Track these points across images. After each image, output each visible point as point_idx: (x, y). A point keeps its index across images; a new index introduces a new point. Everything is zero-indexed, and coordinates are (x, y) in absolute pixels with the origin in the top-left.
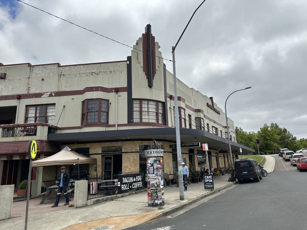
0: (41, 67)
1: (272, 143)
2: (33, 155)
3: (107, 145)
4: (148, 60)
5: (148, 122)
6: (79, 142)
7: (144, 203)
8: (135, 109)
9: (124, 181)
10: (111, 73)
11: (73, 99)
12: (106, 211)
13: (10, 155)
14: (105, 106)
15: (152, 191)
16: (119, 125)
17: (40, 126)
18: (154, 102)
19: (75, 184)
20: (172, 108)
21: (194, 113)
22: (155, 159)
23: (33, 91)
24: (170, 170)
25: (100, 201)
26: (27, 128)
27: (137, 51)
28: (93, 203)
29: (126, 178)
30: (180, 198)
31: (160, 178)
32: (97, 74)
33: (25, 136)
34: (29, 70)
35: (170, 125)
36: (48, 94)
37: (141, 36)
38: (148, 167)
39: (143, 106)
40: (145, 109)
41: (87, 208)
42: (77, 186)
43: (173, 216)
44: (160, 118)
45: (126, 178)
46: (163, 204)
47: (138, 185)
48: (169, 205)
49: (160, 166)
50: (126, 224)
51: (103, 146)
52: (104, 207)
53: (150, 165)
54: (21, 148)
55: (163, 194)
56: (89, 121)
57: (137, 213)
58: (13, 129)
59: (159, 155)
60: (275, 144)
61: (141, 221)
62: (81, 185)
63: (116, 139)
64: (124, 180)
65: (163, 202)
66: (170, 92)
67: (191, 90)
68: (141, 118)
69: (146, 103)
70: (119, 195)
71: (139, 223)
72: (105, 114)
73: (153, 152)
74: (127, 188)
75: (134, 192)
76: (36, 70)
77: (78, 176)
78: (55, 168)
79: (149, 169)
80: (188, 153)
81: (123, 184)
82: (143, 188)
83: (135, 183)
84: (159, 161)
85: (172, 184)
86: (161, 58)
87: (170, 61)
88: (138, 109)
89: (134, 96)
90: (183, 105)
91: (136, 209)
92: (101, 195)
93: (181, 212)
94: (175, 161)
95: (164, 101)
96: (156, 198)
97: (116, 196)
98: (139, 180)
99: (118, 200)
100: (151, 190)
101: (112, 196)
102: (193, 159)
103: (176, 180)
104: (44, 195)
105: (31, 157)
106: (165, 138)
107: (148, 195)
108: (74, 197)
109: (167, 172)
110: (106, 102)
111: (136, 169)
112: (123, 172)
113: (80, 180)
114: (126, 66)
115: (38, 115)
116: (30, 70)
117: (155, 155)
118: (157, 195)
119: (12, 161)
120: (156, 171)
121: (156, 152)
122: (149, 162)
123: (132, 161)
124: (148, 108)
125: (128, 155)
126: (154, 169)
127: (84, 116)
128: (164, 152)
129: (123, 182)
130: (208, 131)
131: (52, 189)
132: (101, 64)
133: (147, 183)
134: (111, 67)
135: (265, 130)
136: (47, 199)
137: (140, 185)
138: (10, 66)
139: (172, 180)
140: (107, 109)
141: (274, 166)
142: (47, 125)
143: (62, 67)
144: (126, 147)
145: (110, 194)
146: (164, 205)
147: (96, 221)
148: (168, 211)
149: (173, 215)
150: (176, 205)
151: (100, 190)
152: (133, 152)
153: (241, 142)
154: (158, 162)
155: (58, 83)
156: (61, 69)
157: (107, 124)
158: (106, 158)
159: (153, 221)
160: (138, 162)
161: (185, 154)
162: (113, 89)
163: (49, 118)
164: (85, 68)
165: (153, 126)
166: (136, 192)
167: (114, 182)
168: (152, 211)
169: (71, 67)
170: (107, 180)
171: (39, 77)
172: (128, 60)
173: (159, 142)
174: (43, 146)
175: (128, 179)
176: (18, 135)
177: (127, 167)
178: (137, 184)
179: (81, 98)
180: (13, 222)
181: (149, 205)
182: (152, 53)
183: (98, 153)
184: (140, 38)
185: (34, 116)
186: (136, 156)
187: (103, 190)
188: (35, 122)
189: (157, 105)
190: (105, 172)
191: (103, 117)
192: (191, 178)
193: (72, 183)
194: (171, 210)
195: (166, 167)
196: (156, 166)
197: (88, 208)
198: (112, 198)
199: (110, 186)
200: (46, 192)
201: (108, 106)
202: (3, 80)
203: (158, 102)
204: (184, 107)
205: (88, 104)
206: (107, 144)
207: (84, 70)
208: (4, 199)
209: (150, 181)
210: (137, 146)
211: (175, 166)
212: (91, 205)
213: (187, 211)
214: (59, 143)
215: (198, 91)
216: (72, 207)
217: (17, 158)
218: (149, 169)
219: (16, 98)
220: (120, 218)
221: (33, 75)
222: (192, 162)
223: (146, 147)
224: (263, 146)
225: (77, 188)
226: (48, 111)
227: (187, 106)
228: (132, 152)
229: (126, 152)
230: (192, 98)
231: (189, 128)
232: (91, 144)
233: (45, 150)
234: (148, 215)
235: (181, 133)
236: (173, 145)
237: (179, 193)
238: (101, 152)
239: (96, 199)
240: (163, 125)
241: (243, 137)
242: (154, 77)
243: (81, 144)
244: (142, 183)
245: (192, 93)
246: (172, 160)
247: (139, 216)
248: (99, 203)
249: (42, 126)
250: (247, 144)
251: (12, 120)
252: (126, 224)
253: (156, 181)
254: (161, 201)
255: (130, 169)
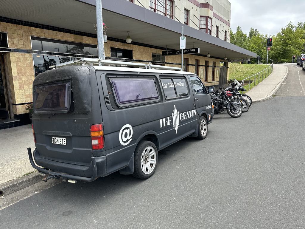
1: (293, 48)
60: (297, 51)
130: (187, 24)
135: (287, 32)
141: (281, 82)
153: (253, 48)
224: (280, 53)
227: (215, 15)
241: (257, 41)
250: (259, 50)
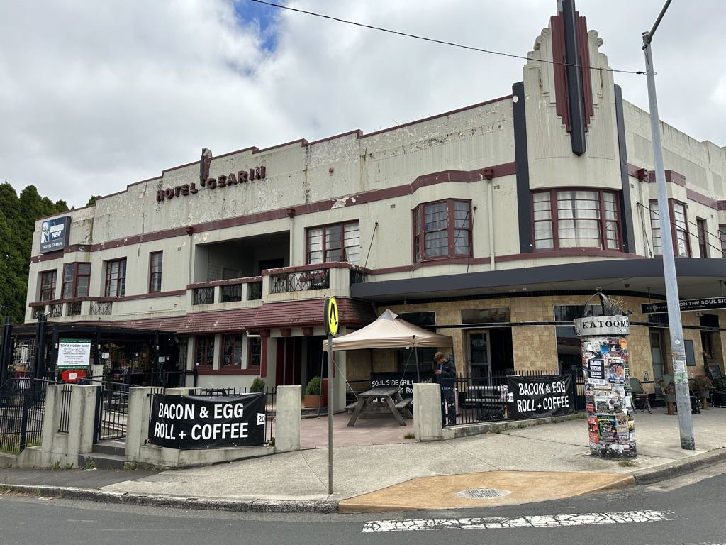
0: (326, 143)
2: (333, 328)
3: (472, 307)
4: (569, 82)
5: (575, 246)
6: (412, 301)
7: (578, 447)
8: (537, 216)
9: (522, 392)
10: (473, 134)
11: (393, 206)
12: (485, 456)
13: (287, 328)
14: (464, 215)
15: (601, 420)
16: (498, 259)
17: (334, 269)
18: (592, 193)
19: (415, 391)
20: (646, 203)
21: (714, 212)
22: (606, 340)
23: (315, 198)
24: (644, 369)
25: (469, 432)
26: (312, 273)
27: (538, 64)
28: (456, 434)
29: (526, 384)
30: (682, 443)
31: (621, 389)
32: (441, 141)
33: (309, 289)
34: (304, 154)
35: (640, 251)
36: (344, 200)
37: (546, 24)
38: (587, 360)
39: (561, 205)
40: (566, 214)
41: (444, 446)
42: (419, 394)
43: (664, 487)
44: (610, 235)
45: (526, 384)
46: (631, 454)
47: (559, 402)
48: (650, 459)
49: (620, 358)
50: (538, 490)
51: (463, 308)
52: (481, 446)
53: (591, 357)
54: (304, 314)
55: (631, 430)
56: (430, 253)
57: (562, 468)
58: (285, 276)
59: (616, 331)
61: (577, 489)
62: (426, 395)
63: (494, 292)
64: (521, 389)
65: (633, 449)
66: (635, 161)
67: (704, 148)
68: (556, 239)
69: (569, 197)
70: (514, 423)
71: (573, 493)
72: (463, 234)
73: (598, 325)
74: (530, 408)
75: (548, 420)
76: (317, 153)
77: (416, 373)
78: (366, 356)
79: (589, 365)
80: (699, 325)
81: (522, 397)
82: (571, 410)
83: (550, 398)
84: (618, 347)
85: (652, 407)
86: (606, 71)
87: (639, 73)
88: (546, 216)
89: (534, 184)
90: (679, 193)
91: (561, 459)
92: (468, 418)
93: (689, 480)
94: (658, 347)
95: (621, 188)
96: (611, 437)
97: (506, 425)
98: (560, 391)
99: (513, 433)
100: (598, 417)
101: (497, 423)
102: (714, 343)
103: (663, 396)
104: (353, 409)
105: (329, 331)
106: (627, 286)
107: (590, 428)
108: (412, 418)
109: (635, 374)
110: (464, 207)
111: (550, 364)
112: (515, 370)
113: (421, 382)
114: (512, 108)
115: (328, 247)
116: (307, 153)
117: (606, 331)
118: (614, 431)
119: (290, 340)
120: (610, 372)
121: (609, 324)
122: (589, 348)
123: (536, 344)
124: (574, 210)
125: (526, 330)
126: (603, 366)
127: (418, 243)
128: (631, 324)
129: (520, 394)
131: (367, 397)
132: (450, 116)
133: (587, 401)
134: (473, 120)
136: (360, 419)
137: (564, 404)
138: (270, 151)
139: (652, 396)
140: (468, 222)
142: (347, 266)
143: (366, 138)
144: (520, 311)
145: (489, 420)
146: (635, 456)
147: (468, 476)
148: (650, 472)
149: (664, 483)
150: (672, 461)
151: (464, 407)
152: (540, 324)
154: (613, 349)
155: (362, 175)
156: (364, 141)
157: (469, 258)
158: (473, 337)
159: (610, 494)
160: (554, 348)
161: (690, 330)
162: (480, 171)
163: (349, 252)
164: (414, 133)
165: (610, 257)
166: (555, 418)
167: (497, 393)
168: (603, 468)
169: (384, 134)
170: (478, 385)
171: (323, 166)
172: (514, 94)
173: (617, 297)
174: (343, 310)
175: (532, 388)
176: (297, 289)
177: (527, 358)
178: (556, 400)
179: (406, 204)
180: (306, 458)
181: (594, 454)
182: (580, 62)
183: (453, 324)
184: (544, 31)
185: (321, 249)
186: (546, 333)
187: (471, 407)
188: (325, 260)
189: (600, 201)
190: (473, 367)
191: (461, 242)
192: (710, 393)
193: (405, 387)
194: (657, 473)
195: (634, 361)
196: (607, 358)
197: (445, 446)
198: (497, 427)
199: (490, 400)
200: (356, 404)
201: (471, 216)
202: (261, 181)
203: (601, 192)
204: (683, 198)
205: (426, 213)
206: (473, 305)
207: (411, 137)
208: (287, 411)
209: (595, 396)
210: (549, 309)
211: (657, 361)
212: (451, 439)
213: (708, 480)
214: (373, 304)
215: (706, 143)
216: (411, 440)
217: (298, 333)
218: (589, 365)
219: (287, 215)
220: (522, 475)
221: (314, 164)
222: (710, 352)
223: (576, 313)
225: (418, 400)
226: (347, 236)
227: (692, 196)
228: (535, 324)
229: (521, 324)
230: (707, 170)
231: (63, 225)
232: (437, 304)
233: (347, 318)
234: (594, 476)
235: (679, 273)
236: (650, 305)
237: (677, 430)
238: (459, 322)
239: (461, 427)
240: (620, 252)
242: (588, 125)
243: (416, 305)
244: (567, 399)
245: (706, 157)
246: (649, 344)
247: (569, 477)
248: (469, 435)
249: (338, 269)
251: (283, 259)
252: (538, 490)
253: (611, 396)
254: (627, 447)
255: (533, 364)
